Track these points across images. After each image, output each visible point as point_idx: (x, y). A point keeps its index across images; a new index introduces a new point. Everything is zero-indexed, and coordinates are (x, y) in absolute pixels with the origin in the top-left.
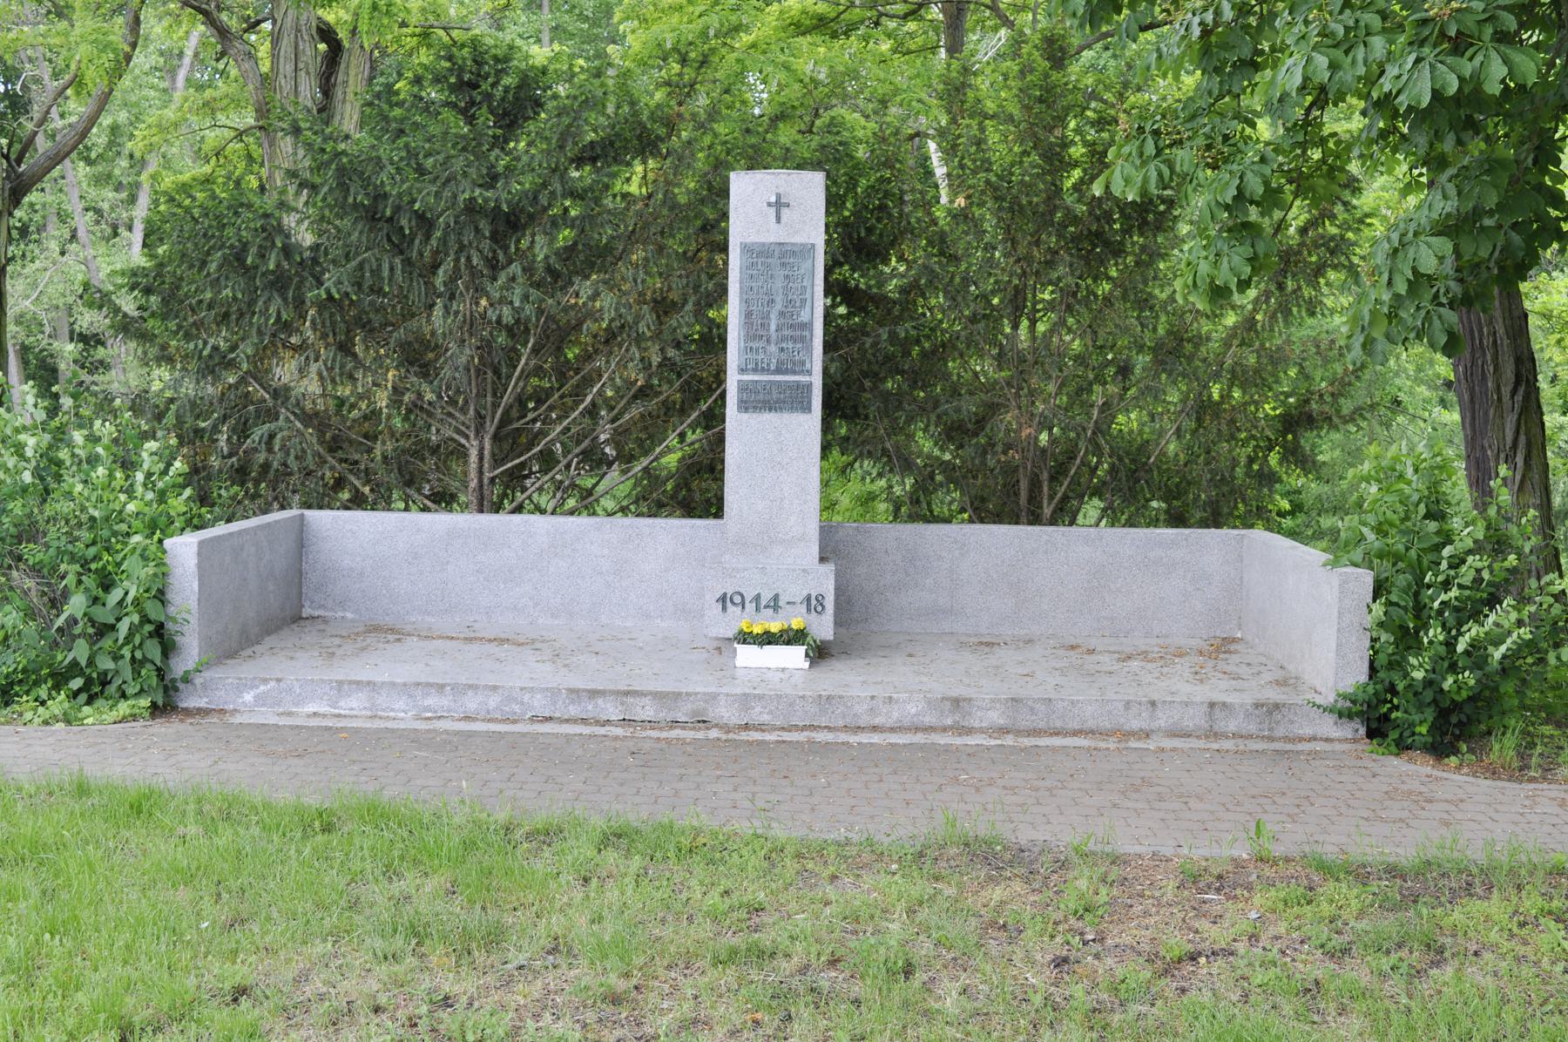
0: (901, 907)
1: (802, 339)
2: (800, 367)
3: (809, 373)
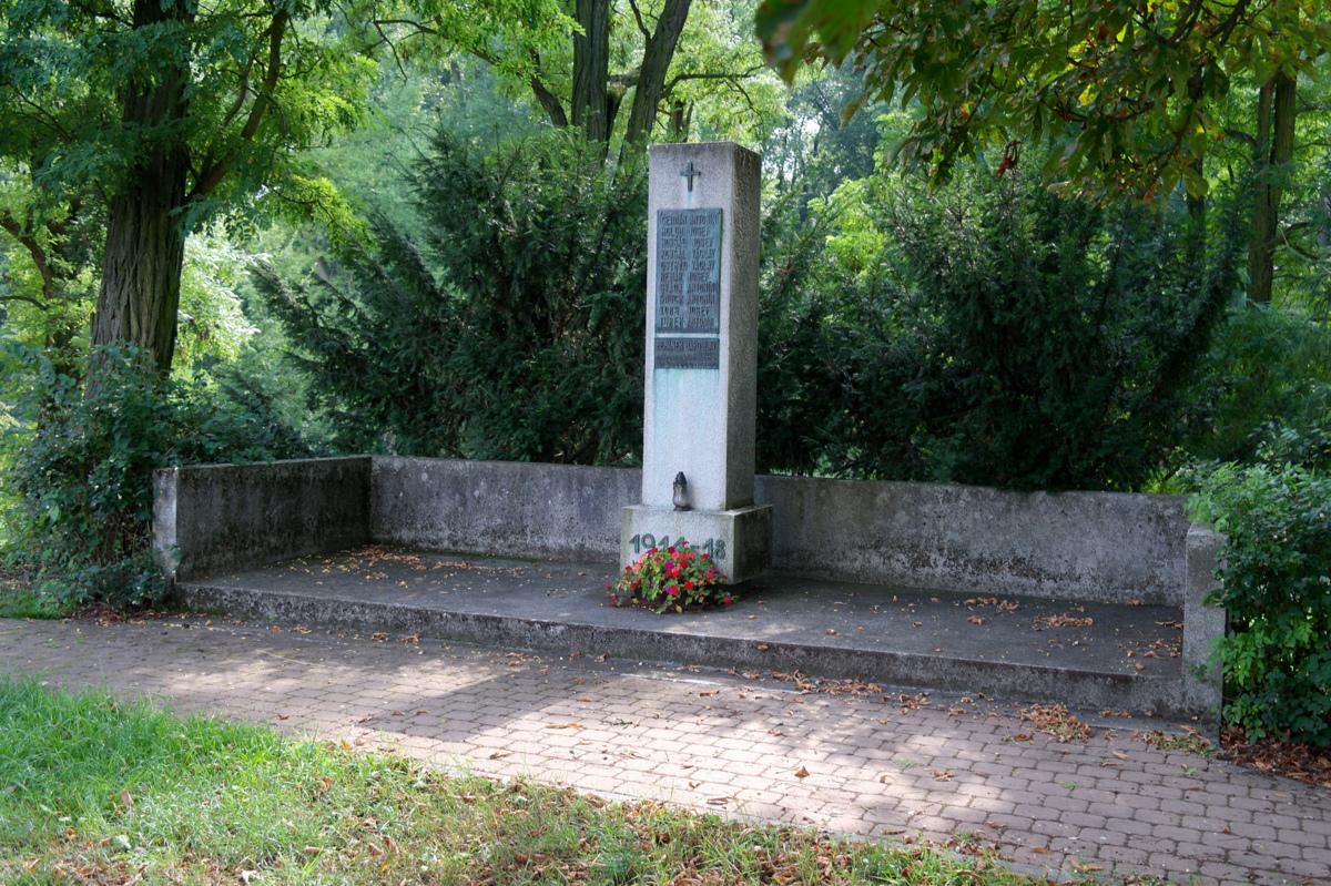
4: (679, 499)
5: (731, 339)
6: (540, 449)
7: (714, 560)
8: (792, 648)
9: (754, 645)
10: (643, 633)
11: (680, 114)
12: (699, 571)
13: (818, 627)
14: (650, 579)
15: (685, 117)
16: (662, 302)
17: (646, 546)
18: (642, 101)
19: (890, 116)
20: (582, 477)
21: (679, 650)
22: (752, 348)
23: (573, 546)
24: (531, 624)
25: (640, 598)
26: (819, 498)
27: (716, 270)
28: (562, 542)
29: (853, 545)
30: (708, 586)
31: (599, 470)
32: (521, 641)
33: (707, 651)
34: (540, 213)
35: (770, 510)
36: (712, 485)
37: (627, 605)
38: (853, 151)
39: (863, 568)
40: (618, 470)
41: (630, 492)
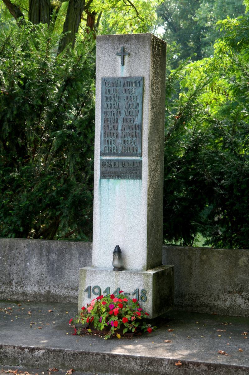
4: (117, 263)
5: (150, 160)
6: (21, 229)
7: (140, 302)
8: (198, 365)
9: (172, 363)
10: (98, 354)
11: (93, 19)
12: (131, 310)
13: (211, 349)
14: (100, 316)
15: (96, 22)
17: (95, 293)
18: (73, 11)
19: (224, 21)
20: (49, 247)
21: (122, 365)
22: (160, 166)
23: (43, 292)
24: (22, 349)
25: (92, 328)
26: (202, 261)
27: (139, 116)
28: (36, 289)
29: (225, 291)
30: (137, 320)
31: (60, 243)
32: (15, 361)
33: (141, 366)
34: (22, 79)
35: (172, 268)
36: (138, 253)
37: (83, 333)
38: (185, 45)
39: (231, 306)
40: (72, 243)
41: (80, 257)
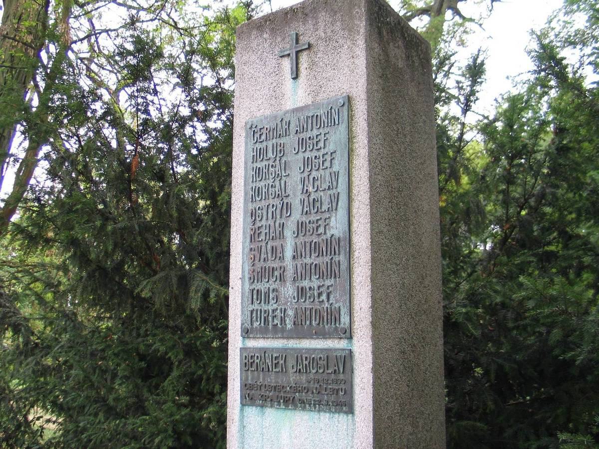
0: (329, 153)
1: (332, 271)
2: (331, 322)
3: (348, 334)
16: (252, 280)
